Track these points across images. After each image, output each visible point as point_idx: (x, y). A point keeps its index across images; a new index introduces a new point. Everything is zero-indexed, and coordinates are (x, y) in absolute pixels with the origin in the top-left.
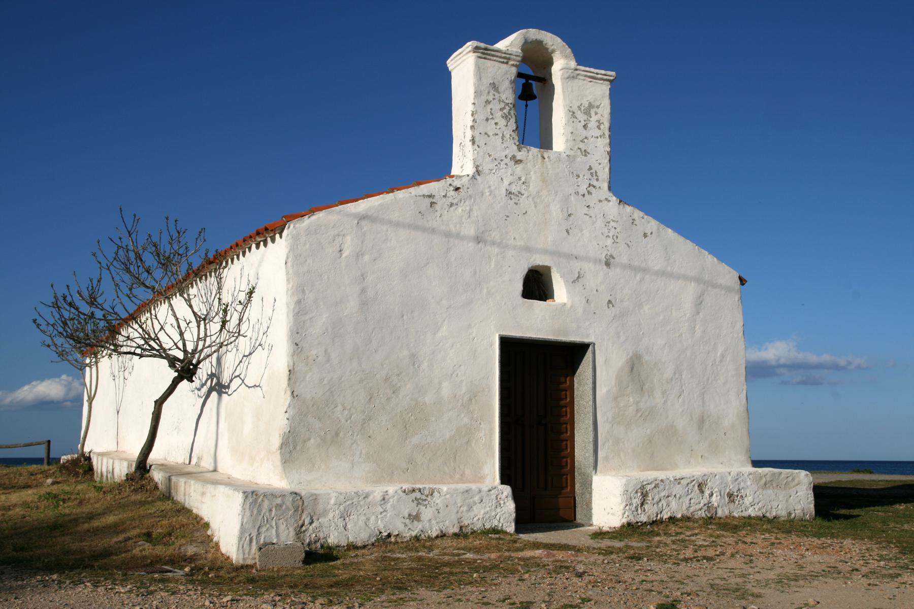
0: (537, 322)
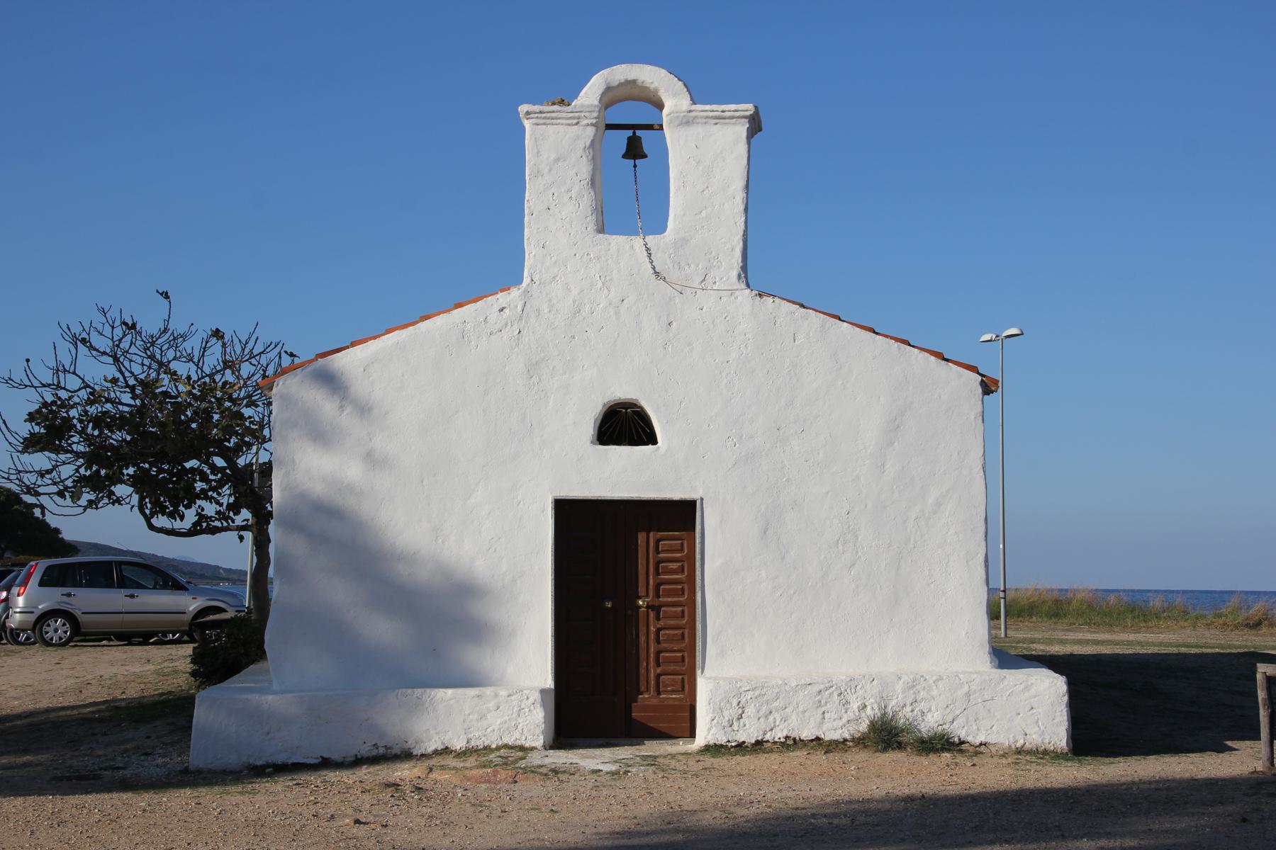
0: (621, 475)
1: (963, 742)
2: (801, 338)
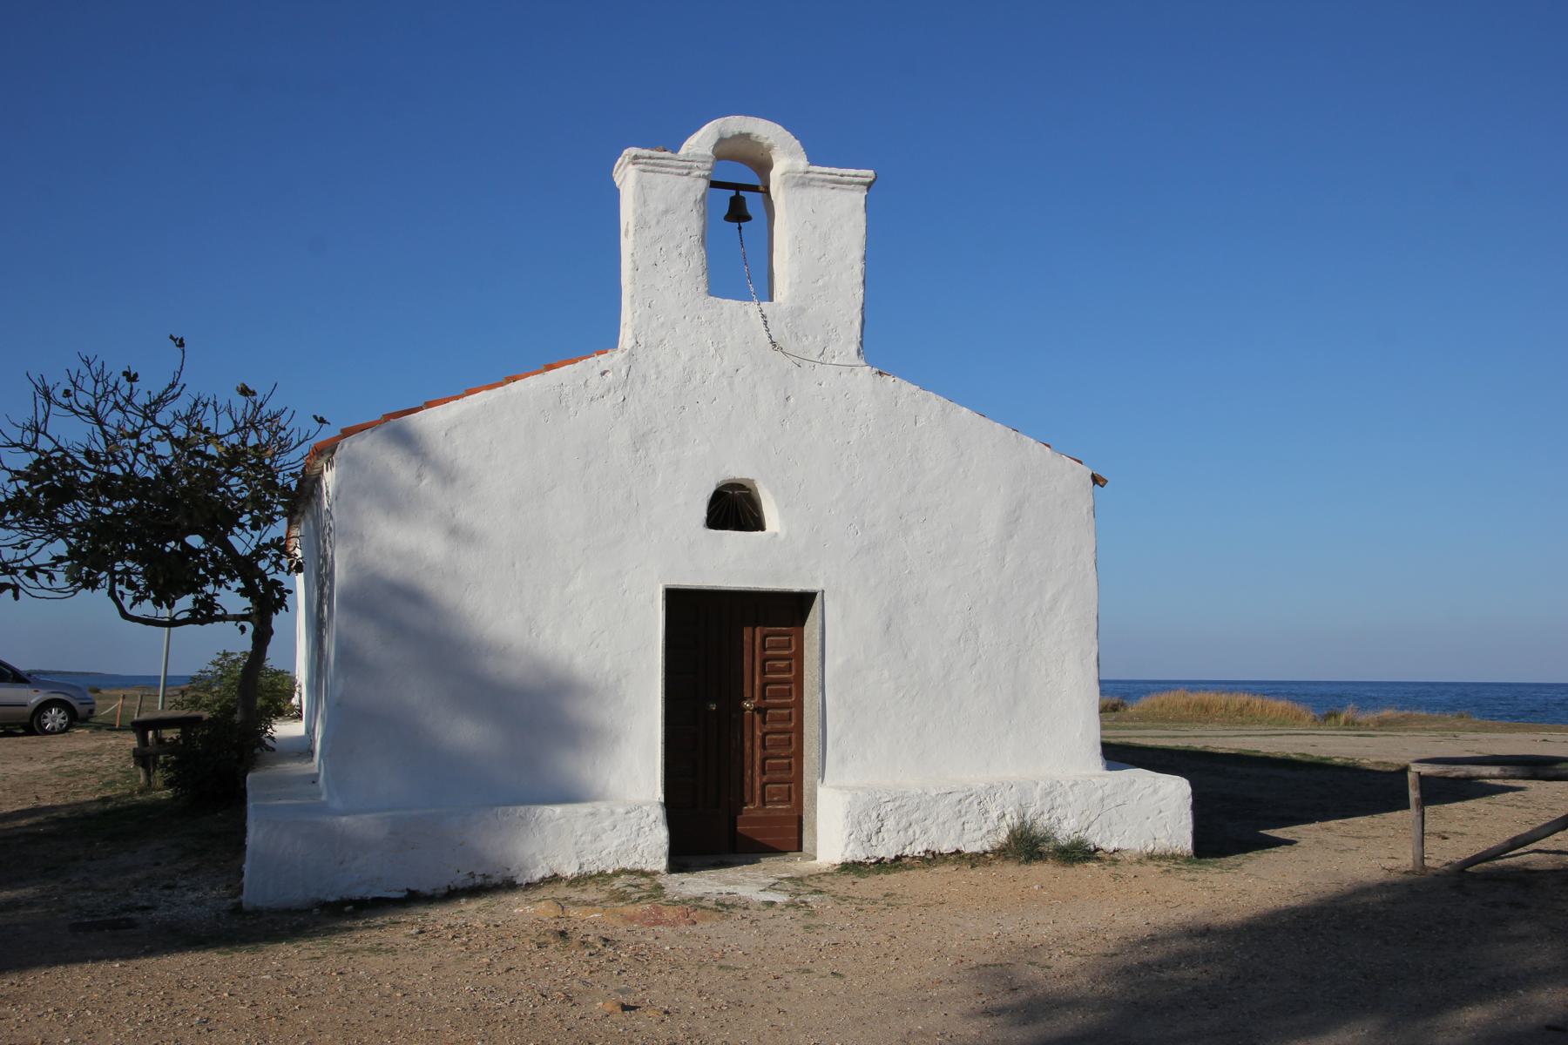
0: (731, 563)
1: (1097, 850)
2: (922, 421)
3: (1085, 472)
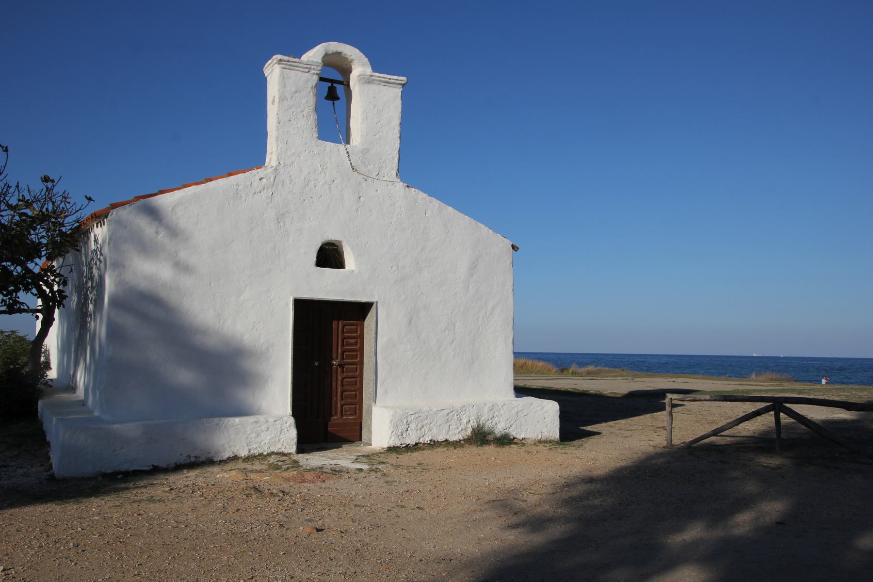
0: (328, 286)
2: (429, 213)
3: (508, 243)
